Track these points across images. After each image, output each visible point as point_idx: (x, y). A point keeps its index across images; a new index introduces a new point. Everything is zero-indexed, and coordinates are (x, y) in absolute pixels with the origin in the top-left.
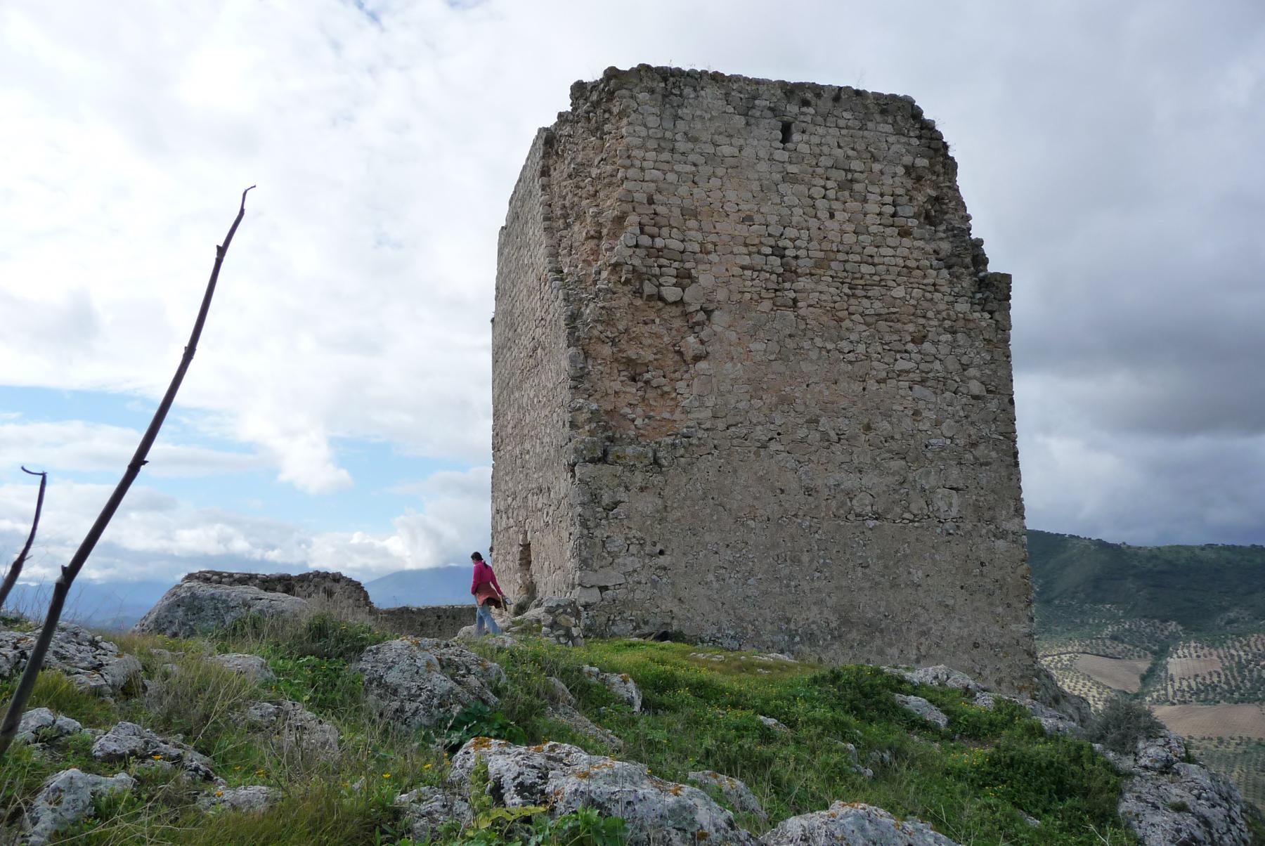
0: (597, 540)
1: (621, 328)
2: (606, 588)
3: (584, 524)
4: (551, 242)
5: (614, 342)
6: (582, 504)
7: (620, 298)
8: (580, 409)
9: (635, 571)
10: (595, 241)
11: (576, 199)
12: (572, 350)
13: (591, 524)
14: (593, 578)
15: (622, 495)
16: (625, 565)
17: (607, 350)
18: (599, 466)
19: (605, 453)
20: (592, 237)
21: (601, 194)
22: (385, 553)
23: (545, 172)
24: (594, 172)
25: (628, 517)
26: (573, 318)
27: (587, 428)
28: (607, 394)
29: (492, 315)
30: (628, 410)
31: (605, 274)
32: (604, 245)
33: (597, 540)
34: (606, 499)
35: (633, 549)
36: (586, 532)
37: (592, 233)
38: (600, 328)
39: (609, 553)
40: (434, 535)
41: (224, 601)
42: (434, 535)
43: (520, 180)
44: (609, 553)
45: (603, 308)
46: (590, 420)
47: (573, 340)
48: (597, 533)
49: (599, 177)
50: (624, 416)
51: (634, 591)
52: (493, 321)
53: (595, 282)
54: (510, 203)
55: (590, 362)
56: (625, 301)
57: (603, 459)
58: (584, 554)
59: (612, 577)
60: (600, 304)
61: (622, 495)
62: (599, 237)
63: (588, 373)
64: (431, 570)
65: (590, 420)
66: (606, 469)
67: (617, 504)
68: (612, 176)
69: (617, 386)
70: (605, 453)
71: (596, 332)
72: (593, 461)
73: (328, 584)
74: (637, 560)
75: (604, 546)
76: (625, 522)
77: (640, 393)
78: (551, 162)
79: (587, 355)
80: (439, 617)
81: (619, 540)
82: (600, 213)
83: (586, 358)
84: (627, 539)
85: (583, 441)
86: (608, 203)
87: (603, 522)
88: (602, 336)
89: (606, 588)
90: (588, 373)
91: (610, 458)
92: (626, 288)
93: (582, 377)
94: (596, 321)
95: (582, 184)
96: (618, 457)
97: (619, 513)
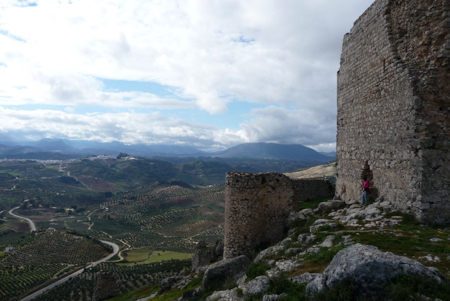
0: (430, 182)
1: (440, 86)
2: (433, 203)
3: (424, 175)
4: (392, 44)
5: (435, 93)
6: (423, 167)
7: (440, 73)
8: (421, 124)
9: (446, 196)
10: (427, 46)
11: (416, 27)
12: (415, 97)
13: (427, 175)
14: (427, 199)
15: (441, 163)
16: (441, 193)
17: (432, 97)
18: (431, 150)
19: (434, 145)
20: (426, 44)
21: (431, 24)
22: (239, 137)
23: (388, 12)
24: (428, 14)
25: (443, 172)
26: (415, 83)
27: (424, 132)
28: (431, 117)
29: (338, 70)
30: (440, 123)
31: (432, 62)
32: (432, 48)
33: (430, 182)
34: (434, 164)
35: (445, 186)
36: (424, 179)
37: (426, 42)
38: (430, 87)
39: (434, 188)
40: (256, 131)
41: (390, 266)
42: (256, 131)
43: (364, 14)
44: (434, 188)
45: (431, 78)
46: (426, 130)
47: (416, 92)
48: (430, 179)
49: (431, 16)
50: (438, 126)
51: (445, 204)
52: (338, 72)
53: (426, 66)
54: (355, 24)
55: (424, 102)
56: (443, 74)
57: (433, 147)
58: (424, 188)
59: (436, 198)
60: (430, 76)
61: (441, 163)
62: (430, 44)
63: (423, 107)
64: (255, 144)
65: (426, 130)
66: (434, 152)
67: (438, 167)
68: (438, 15)
69: (436, 113)
70: (434, 145)
71: (428, 89)
72: (429, 148)
73: (277, 177)
74: (447, 191)
75: (432, 185)
76: (442, 175)
77: (445, 116)
78: (392, 7)
79: (422, 99)
80: (303, 183)
81: (439, 183)
82: (431, 33)
83: (422, 100)
84: (443, 182)
85: (424, 139)
86: (436, 28)
87: (432, 174)
88: (431, 91)
89: (433, 203)
90: (423, 107)
91: (436, 147)
92: (444, 69)
93: (420, 109)
94: (428, 84)
95: (421, 19)
96: (440, 146)
97: (440, 171)
